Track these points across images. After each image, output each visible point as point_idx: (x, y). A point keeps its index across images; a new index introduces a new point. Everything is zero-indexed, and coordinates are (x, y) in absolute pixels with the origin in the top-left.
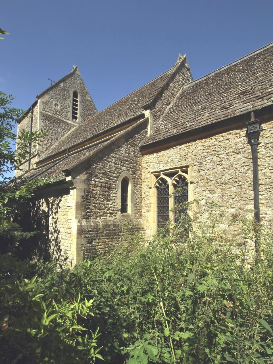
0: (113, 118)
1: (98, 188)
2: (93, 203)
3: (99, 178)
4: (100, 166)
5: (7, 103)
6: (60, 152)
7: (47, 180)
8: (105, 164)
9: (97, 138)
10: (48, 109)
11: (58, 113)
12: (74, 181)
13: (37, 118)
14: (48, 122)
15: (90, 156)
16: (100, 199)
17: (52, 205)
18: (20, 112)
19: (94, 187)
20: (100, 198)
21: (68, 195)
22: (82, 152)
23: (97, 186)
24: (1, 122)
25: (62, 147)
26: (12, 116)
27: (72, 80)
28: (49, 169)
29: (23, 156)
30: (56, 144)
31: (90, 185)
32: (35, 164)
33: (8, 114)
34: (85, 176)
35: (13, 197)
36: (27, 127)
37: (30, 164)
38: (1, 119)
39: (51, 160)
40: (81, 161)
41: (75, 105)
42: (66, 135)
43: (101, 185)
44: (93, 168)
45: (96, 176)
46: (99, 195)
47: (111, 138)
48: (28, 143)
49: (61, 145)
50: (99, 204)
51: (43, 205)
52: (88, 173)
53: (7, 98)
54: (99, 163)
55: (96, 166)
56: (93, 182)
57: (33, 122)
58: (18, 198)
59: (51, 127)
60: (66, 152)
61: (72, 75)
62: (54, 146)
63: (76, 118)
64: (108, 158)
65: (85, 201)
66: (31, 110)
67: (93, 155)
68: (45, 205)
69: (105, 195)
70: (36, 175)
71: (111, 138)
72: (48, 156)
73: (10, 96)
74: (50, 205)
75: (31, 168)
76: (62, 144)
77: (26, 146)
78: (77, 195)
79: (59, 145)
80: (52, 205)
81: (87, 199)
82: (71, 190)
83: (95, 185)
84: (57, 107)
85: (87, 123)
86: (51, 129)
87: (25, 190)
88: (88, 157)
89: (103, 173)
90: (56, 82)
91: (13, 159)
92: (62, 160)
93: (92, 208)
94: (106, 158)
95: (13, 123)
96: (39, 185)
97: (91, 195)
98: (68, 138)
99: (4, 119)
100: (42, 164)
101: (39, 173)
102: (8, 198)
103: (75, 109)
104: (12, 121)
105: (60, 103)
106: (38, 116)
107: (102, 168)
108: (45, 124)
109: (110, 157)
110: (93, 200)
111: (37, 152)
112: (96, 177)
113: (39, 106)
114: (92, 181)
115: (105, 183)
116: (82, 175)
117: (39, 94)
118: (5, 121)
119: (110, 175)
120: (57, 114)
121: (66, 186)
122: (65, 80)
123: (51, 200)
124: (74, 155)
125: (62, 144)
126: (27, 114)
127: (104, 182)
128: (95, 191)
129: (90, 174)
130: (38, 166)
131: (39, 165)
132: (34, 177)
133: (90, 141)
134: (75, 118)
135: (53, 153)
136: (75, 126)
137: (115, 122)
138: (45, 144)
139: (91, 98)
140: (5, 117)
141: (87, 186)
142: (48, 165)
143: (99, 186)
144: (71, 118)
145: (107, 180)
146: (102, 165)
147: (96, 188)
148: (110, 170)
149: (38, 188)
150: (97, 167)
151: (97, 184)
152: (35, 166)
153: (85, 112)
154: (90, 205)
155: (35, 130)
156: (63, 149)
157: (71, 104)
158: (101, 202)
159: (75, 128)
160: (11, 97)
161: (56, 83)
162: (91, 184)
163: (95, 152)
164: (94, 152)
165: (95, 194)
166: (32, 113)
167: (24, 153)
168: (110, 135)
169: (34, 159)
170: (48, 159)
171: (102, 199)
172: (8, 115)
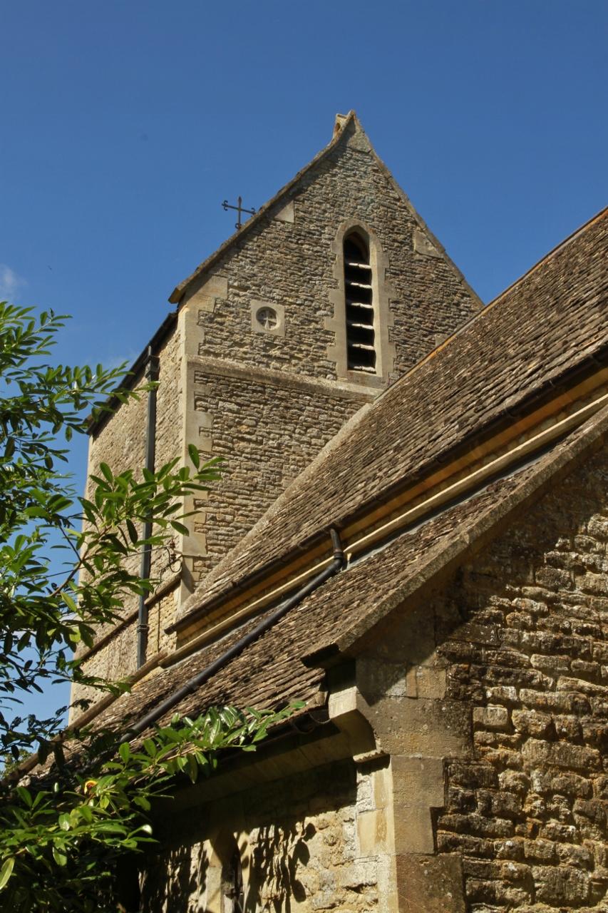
0: (574, 317)
1: (532, 750)
2: (507, 856)
3: (527, 683)
4: (528, 601)
5: (34, 348)
6: (296, 548)
7: (224, 727)
8: (555, 589)
9: (491, 444)
10: (227, 343)
11: (275, 352)
12: (372, 714)
13: (176, 393)
14: (227, 405)
15: (460, 548)
16: (553, 823)
17: (258, 879)
18: (88, 380)
19: (507, 743)
20: (556, 814)
21: (347, 811)
22: (413, 532)
23: (525, 735)
24: (6, 441)
25: (305, 519)
26: (52, 404)
27: (337, 179)
28: (238, 653)
29: (99, 604)
30: (273, 510)
31: (479, 734)
32: (168, 631)
33: (36, 398)
34: (443, 674)
35: (40, 850)
36: (131, 449)
37: (144, 633)
38: (6, 429)
39: (248, 602)
40: (407, 586)
41: (356, 295)
42: (324, 454)
43: (551, 726)
44: (487, 622)
45: (511, 671)
46: (547, 795)
47: (573, 427)
48: (125, 528)
49: (298, 510)
50: (554, 860)
51: (204, 877)
52: (454, 658)
53: (31, 326)
54: (521, 583)
55: (501, 607)
56: (495, 714)
57: (159, 420)
58: (67, 854)
59: (244, 428)
60: (324, 546)
61: (331, 159)
62: (264, 523)
63: (369, 358)
64: (574, 549)
65: (453, 844)
66: (147, 364)
67: (475, 540)
68: (214, 876)
69: (588, 796)
70: (176, 695)
71: (573, 427)
72: (236, 579)
73: (44, 317)
74: (246, 874)
75: (151, 654)
76: (303, 506)
77: (119, 547)
78: (398, 809)
79: (288, 514)
80: (258, 879)
81: (466, 828)
82: (360, 777)
83: (509, 728)
84: (272, 324)
85: (429, 371)
86: (243, 439)
87: (105, 803)
88: (448, 559)
89: (554, 648)
90: (257, 211)
91: (51, 626)
92: (308, 593)
93: (509, 894)
94: (562, 549)
95: (57, 442)
96: (184, 761)
97: (488, 801)
98: (332, 467)
99: (15, 427)
100: (204, 628)
101: (189, 683)
102: (18, 858)
103: (357, 315)
104: (55, 431)
105: (284, 303)
106: (183, 384)
107: (544, 614)
108: (217, 416)
109: (586, 539)
110: (510, 833)
111: (177, 566)
112: (508, 675)
113: (183, 338)
114: (490, 707)
115: (575, 710)
116: (422, 671)
117: (181, 284)
118: (21, 434)
119: (600, 655)
120: (269, 357)
121: (329, 748)
122: (301, 191)
123: (248, 841)
124: (373, 554)
125: (303, 506)
126: (129, 383)
127: (568, 705)
128: (515, 767)
129: (473, 659)
130: (186, 639)
131: (191, 636)
132: (163, 704)
133: (455, 466)
134: (360, 358)
135: (258, 557)
136: (365, 399)
137: (583, 333)
138: (219, 517)
139: (435, 242)
140: (24, 416)
141: (460, 742)
142: (234, 632)
143: (536, 736)
144: (342, 363)
145: (581, 690)
146: (537, 597)
147: (517, 746)
148: (598, 622)
149: (179, 780)
150: (511, 609)
151: (523, 720)
152: (169, 645)
153: (415, 321)
154: (489, 873)
155: (169, 454)
156: (308, 529)
157: (337, 297)
158: (565, 847)
159: (366, 408)
160: (49, 321)
161: (258, 213)
162: (481, 727)
163: (485, 520)
164: (480, 524)
165: (513, 789)
166: (154, 376)
167: (103, 584)
168: (566, 410)
169: (163, 603)
170: (236, 595)
171: (569, 820)
172: (33, 406)
